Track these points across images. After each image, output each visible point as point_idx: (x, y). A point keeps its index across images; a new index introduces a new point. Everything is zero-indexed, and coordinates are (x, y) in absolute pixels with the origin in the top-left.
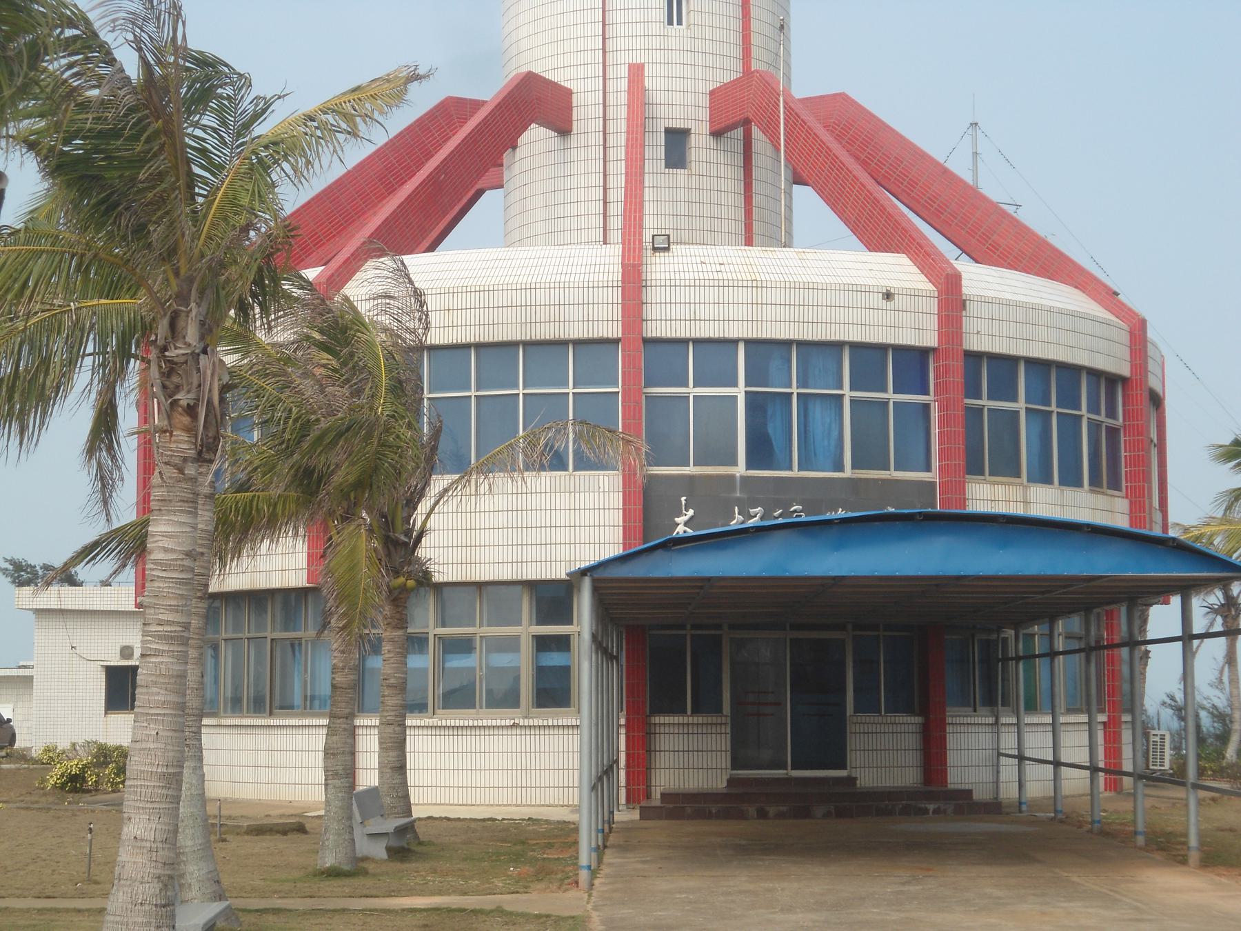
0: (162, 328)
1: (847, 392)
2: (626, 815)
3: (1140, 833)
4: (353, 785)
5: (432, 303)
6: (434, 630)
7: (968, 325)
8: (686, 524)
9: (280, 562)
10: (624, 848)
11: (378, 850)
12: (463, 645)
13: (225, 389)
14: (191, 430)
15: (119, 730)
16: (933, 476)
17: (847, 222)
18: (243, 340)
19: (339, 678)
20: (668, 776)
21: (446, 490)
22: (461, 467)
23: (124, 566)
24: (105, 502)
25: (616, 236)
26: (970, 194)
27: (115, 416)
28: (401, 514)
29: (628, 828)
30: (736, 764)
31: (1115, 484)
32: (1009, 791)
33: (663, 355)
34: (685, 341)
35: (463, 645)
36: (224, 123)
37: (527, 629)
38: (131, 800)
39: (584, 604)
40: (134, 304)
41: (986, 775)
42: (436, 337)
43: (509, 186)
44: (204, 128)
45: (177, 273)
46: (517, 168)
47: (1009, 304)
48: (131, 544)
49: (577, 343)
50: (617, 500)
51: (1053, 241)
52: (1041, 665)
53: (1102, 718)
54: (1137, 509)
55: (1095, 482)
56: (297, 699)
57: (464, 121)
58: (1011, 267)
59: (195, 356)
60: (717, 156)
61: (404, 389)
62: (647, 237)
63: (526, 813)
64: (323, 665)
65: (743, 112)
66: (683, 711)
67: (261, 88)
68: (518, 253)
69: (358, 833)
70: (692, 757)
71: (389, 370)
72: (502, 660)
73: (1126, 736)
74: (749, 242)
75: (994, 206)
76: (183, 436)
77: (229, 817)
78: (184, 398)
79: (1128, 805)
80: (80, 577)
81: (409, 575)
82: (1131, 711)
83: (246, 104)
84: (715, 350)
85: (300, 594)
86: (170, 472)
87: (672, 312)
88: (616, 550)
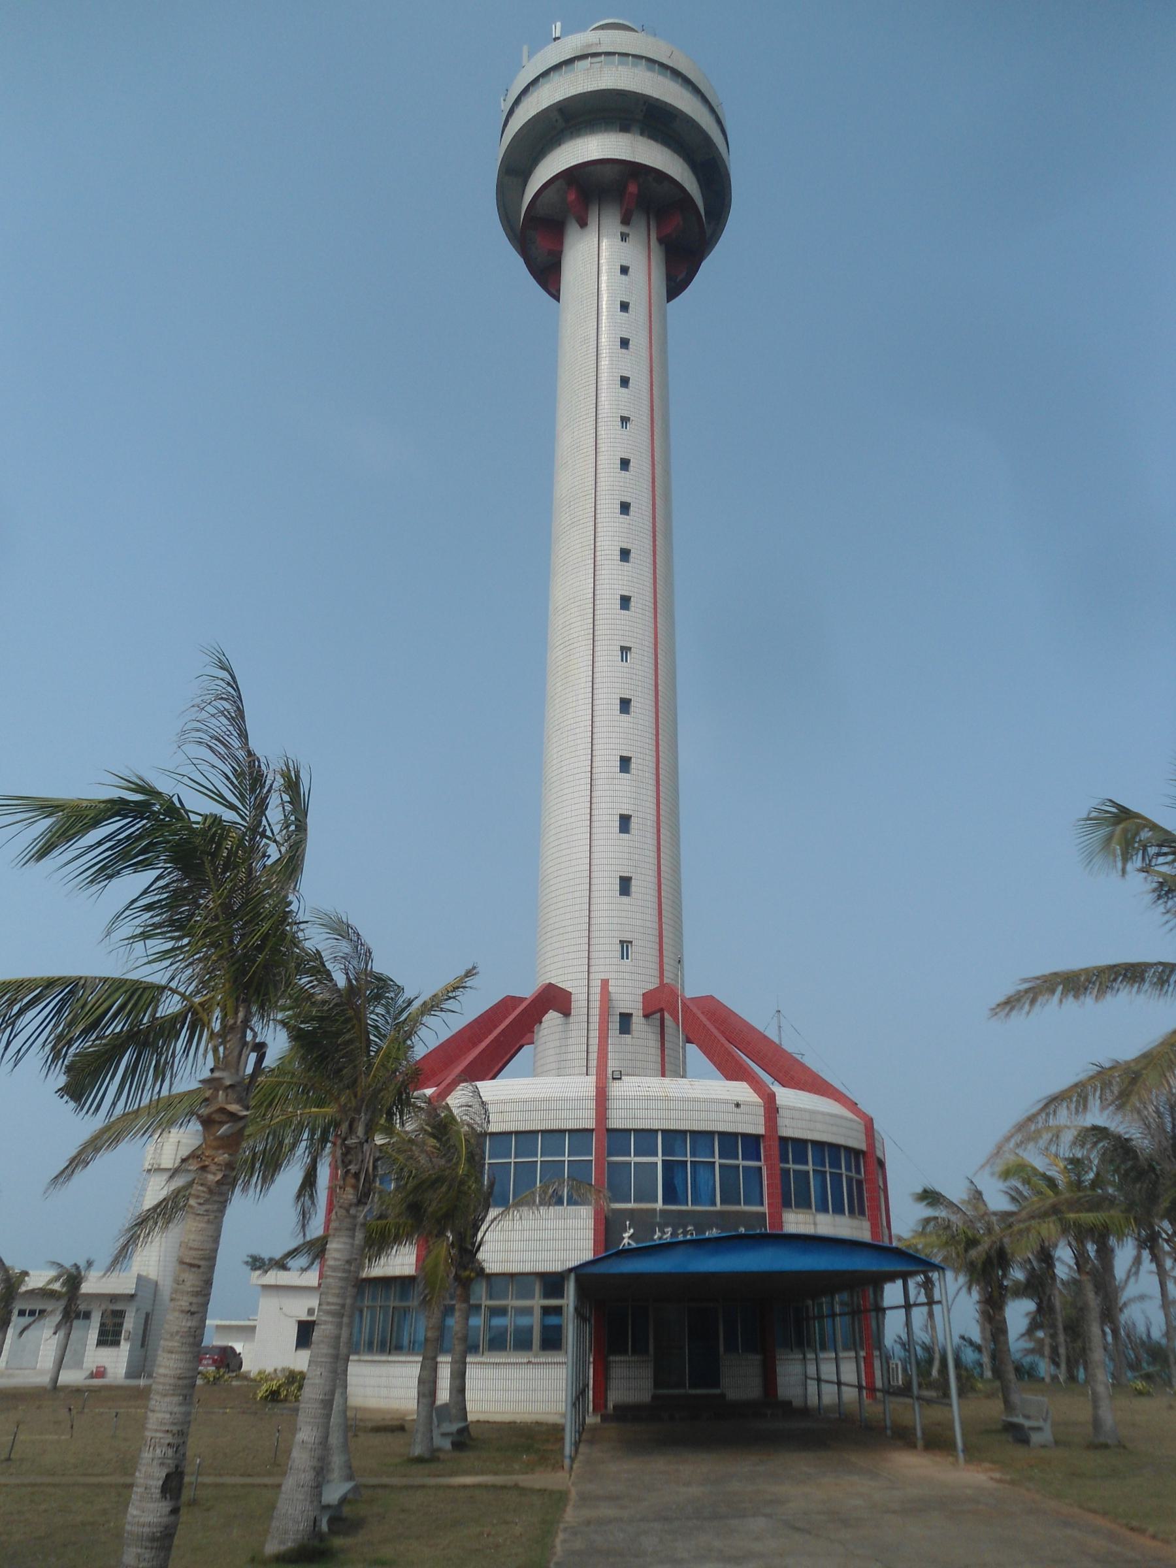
0: (345, 1127)
1: (717, 1160)
2: (592, 1420)
3: (879, 1390)
4: (434, 1402)
5: (491, 1108)
6: (486, 1302)
7: (781, 1122)
8: (629, 1238)
9: (401, 1261)
10: (591, 1442)
11: (447, 1444)
12: (502, 1311)
13: (376, 1160)
14: (355, 1187)
15: (300, 1361)
16: (765, 1209)
17: (714, 1064)
18: (389, 1130)
19: (429, 1334)
20: (615, 1396)
21: (495, 1219)
22: (504, 1202)
23: (312, 1263)
24: (304, 1226)
25: (593, 1070)
26: (778, 1049)
27: (315, 1176)
28: (470, 1233)
29: (594, 1429)
30: (658, 1384)
31: (862, 1213)
32: (813, 1400)
33: (617, 1138)
34: (629, 1131)
35: (502, 1311)
36: (388, 1012)
37: (538, 1302)
38: (302, 1418)
39: (571, 1288)
40: (330, 1110)
41: (799, 1391)
42: (493, 1128)
43: (538, 1043)
44: (377, 1015)
45: (356, 1096)
46: (541, 1034)
47: (800, 1110)
48: (316, 1249)
49: (571, 1131)
50: (591, 1223)
51: (821, 1074)
52: (827, 1322)
53: (862, 1354)
54: (875, 1228)
55: (852, 1211)
56: (406, 1342)
57: (514, 1009)
59: (361, 1144)
60: (646, 1028)
61: (474, 1159)
62: (610, 1071)
63: (507, 1418)
64: (420, 1326)
65: (660, 1005)
66: (625, 1352)
67: (408, 994)
69: (436, 1433)
70: (631, 1384)
71: (467, 1148)
72: (524, 1321)
73: (877, 1364)
74: (663, 1075)
75: (789, 1054)
76: (349, 1190)
77: (361, 1420)
78: (353, 1168)
79: (880, 1408)
80: (289, 1265)
81: (472, 1270)
82: (879, 1349)
83: (400, 1002)
84: (646, 1136)
85: (411, 1279)
86: (342, 1212)
87: (622, 1113)
88: (588, 1256)
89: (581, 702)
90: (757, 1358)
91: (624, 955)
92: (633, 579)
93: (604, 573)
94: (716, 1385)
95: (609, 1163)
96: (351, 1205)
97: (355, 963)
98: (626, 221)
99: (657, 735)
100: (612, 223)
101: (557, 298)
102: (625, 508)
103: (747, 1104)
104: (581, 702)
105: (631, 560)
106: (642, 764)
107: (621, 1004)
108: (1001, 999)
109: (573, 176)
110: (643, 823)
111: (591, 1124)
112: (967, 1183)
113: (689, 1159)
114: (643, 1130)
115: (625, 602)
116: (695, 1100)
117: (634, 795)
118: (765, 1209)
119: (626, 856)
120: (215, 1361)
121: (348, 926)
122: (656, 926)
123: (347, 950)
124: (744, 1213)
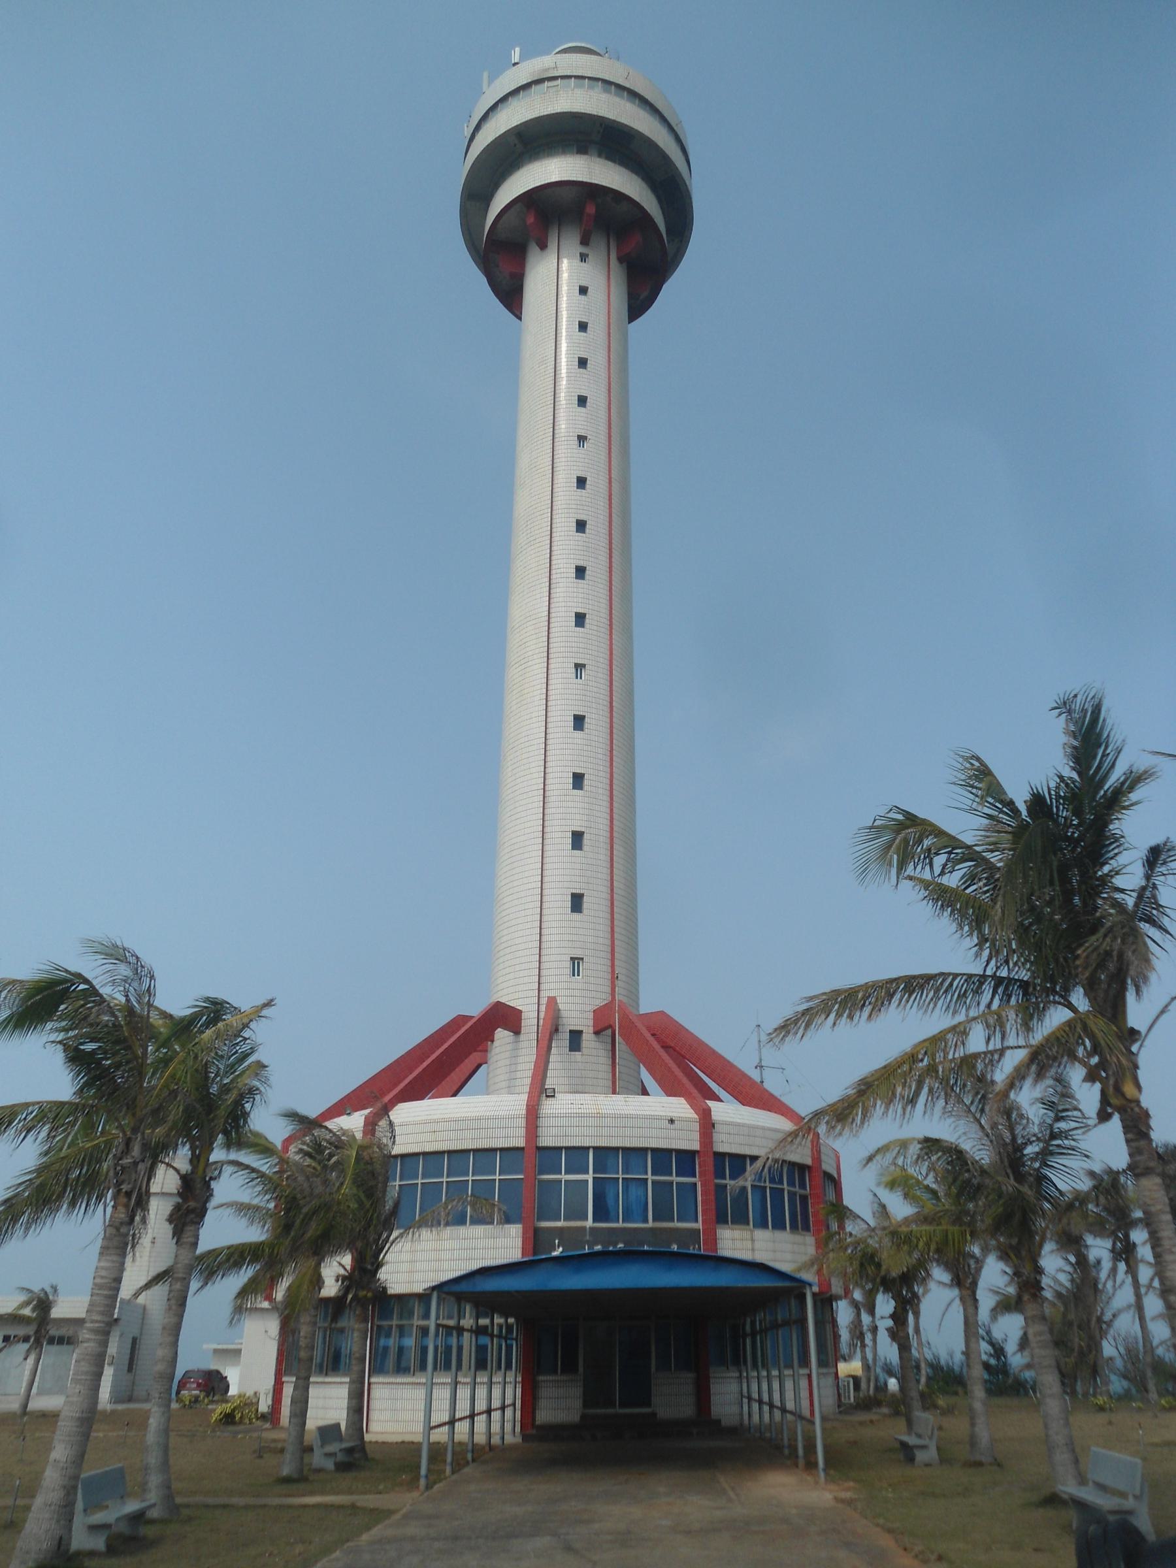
5: (398, 1130)
7: (717, 1137)
11: (330, 1465)
14: (126, 1206)
16: (699, 1225)
20: (544, 1416)
30: (586, 1405)
31: (806, 1228)
33: (548, 1156)
34: (560, 1148)
46: (493, 1053)
47: (739, 1125)
49: (502, 1150)
58: (756, 1106)
60: (598, 1045)
63: (399, 1439)
68: (493, 1098)
74: (614, 1092)
84: (576, 1154)
87: (554, 1131)
89: (534, 720)
90: (690, 1376)
91: (575, 972)
92: (590, 596)
93: (559, 592)
94: (649, 1405)
95: (540, 1181)
96: (121, 1223)
97: (135, 984)
98: (585, 242)
99: (611, 751)
100: (572, 242)
101: (520, 318)
102: (581, 526)
103: (682, 1120)
104: (534, 720)
105: (587, 577)
106: (596, 782)
107: (572, 1021)
108: (779, 1022)
109: (531, 199)
110: (596, 840)
111: (520, 1142)
112: (871, 1196)
113: (620, 1176)
114: (574, 1148)
115: (580, 619)
116: (627, 1117)
117: (587, 812)
118: (699, 1225)
119: (577, 872)
120: (199, 1385)
121: (124, 949)
122: (608, 942)
123: (125, 973)
124: (677, 1230)
